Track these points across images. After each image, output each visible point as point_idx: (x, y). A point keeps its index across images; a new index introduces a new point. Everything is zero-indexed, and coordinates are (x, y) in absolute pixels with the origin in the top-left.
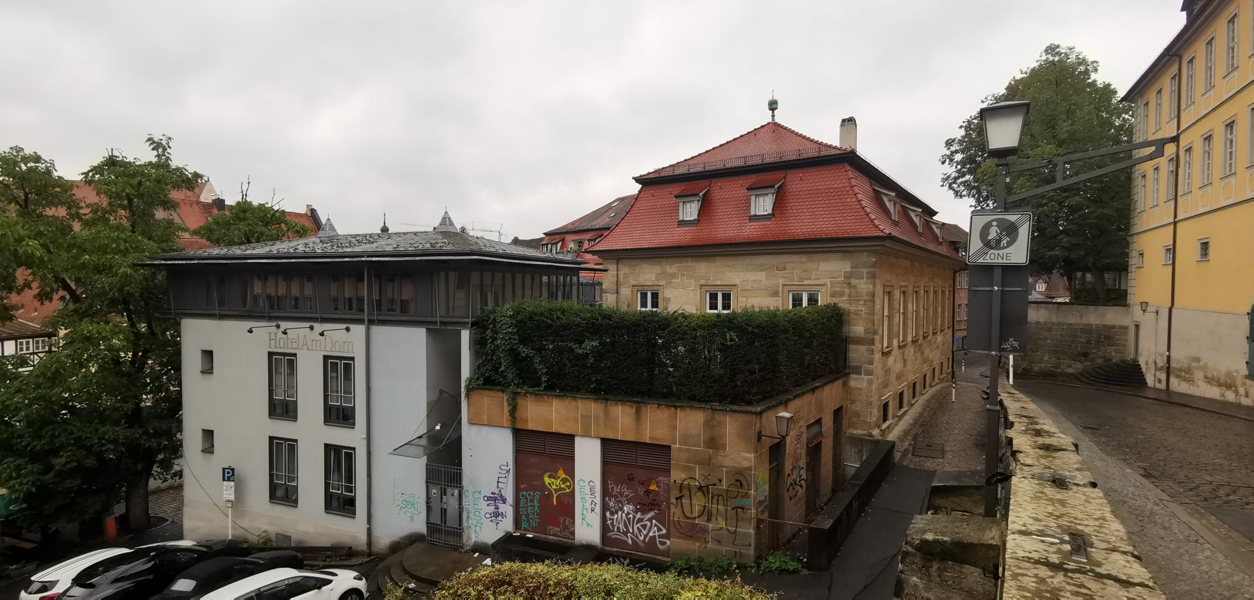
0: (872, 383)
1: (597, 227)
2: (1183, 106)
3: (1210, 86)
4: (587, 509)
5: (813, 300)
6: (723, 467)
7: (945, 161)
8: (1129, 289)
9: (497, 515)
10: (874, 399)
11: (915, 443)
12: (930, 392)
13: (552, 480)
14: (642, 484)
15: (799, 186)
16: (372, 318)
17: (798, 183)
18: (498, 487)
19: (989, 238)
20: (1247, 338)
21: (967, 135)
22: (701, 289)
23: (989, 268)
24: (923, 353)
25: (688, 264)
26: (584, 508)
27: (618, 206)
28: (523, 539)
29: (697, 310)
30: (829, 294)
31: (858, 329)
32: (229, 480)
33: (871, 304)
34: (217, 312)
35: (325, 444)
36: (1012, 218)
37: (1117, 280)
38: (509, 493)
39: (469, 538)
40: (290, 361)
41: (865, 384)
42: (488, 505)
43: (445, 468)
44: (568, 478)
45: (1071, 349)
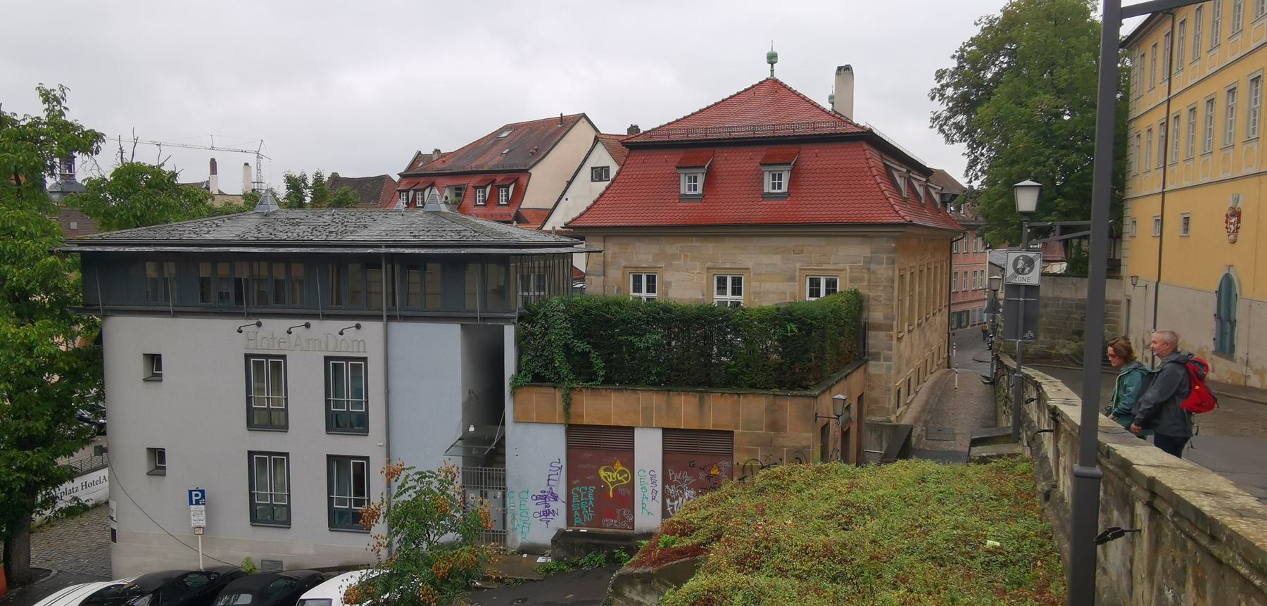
0: (891, 369)
1: (486, 168)
2: (1174, 71)
3: (1196, 58)
4: (647, 498)
5: (831, 285)
6: (783, 447)
7: (935, 96)
8: (1122, 259)
9: (547, 513)
10: (892, 385)
11: (926, 428)
12: (931, 379)
13: (609, 473)
14: (704, 469)
15: (814, 163)
16: (393, 313)
17: (812, 158)
18: (548, 485)
19: (1018, 267)
20: (1215, 315)
21: (960, 67)
22: (708, 272)
23: (1017, 286)
24: (925, 337)
25: (694, 244)
26: (644, 497)
27: (510, 138)
28: (577, 534)
29: (703, 295)
30: (848, 279)
31: (876, 315)
32: (197, 503)
33: (890, 290)
34: (320, 311)
35: (327, 455)
36: (1031, 255)
37: (1112, 249)
38: (562, 492)
39: (514, 540)
40: (278, 364)
41: (884, 371)
42: (537, 504)
43: (486, 470)
44: (627, 471)
45: (1066, 327)
